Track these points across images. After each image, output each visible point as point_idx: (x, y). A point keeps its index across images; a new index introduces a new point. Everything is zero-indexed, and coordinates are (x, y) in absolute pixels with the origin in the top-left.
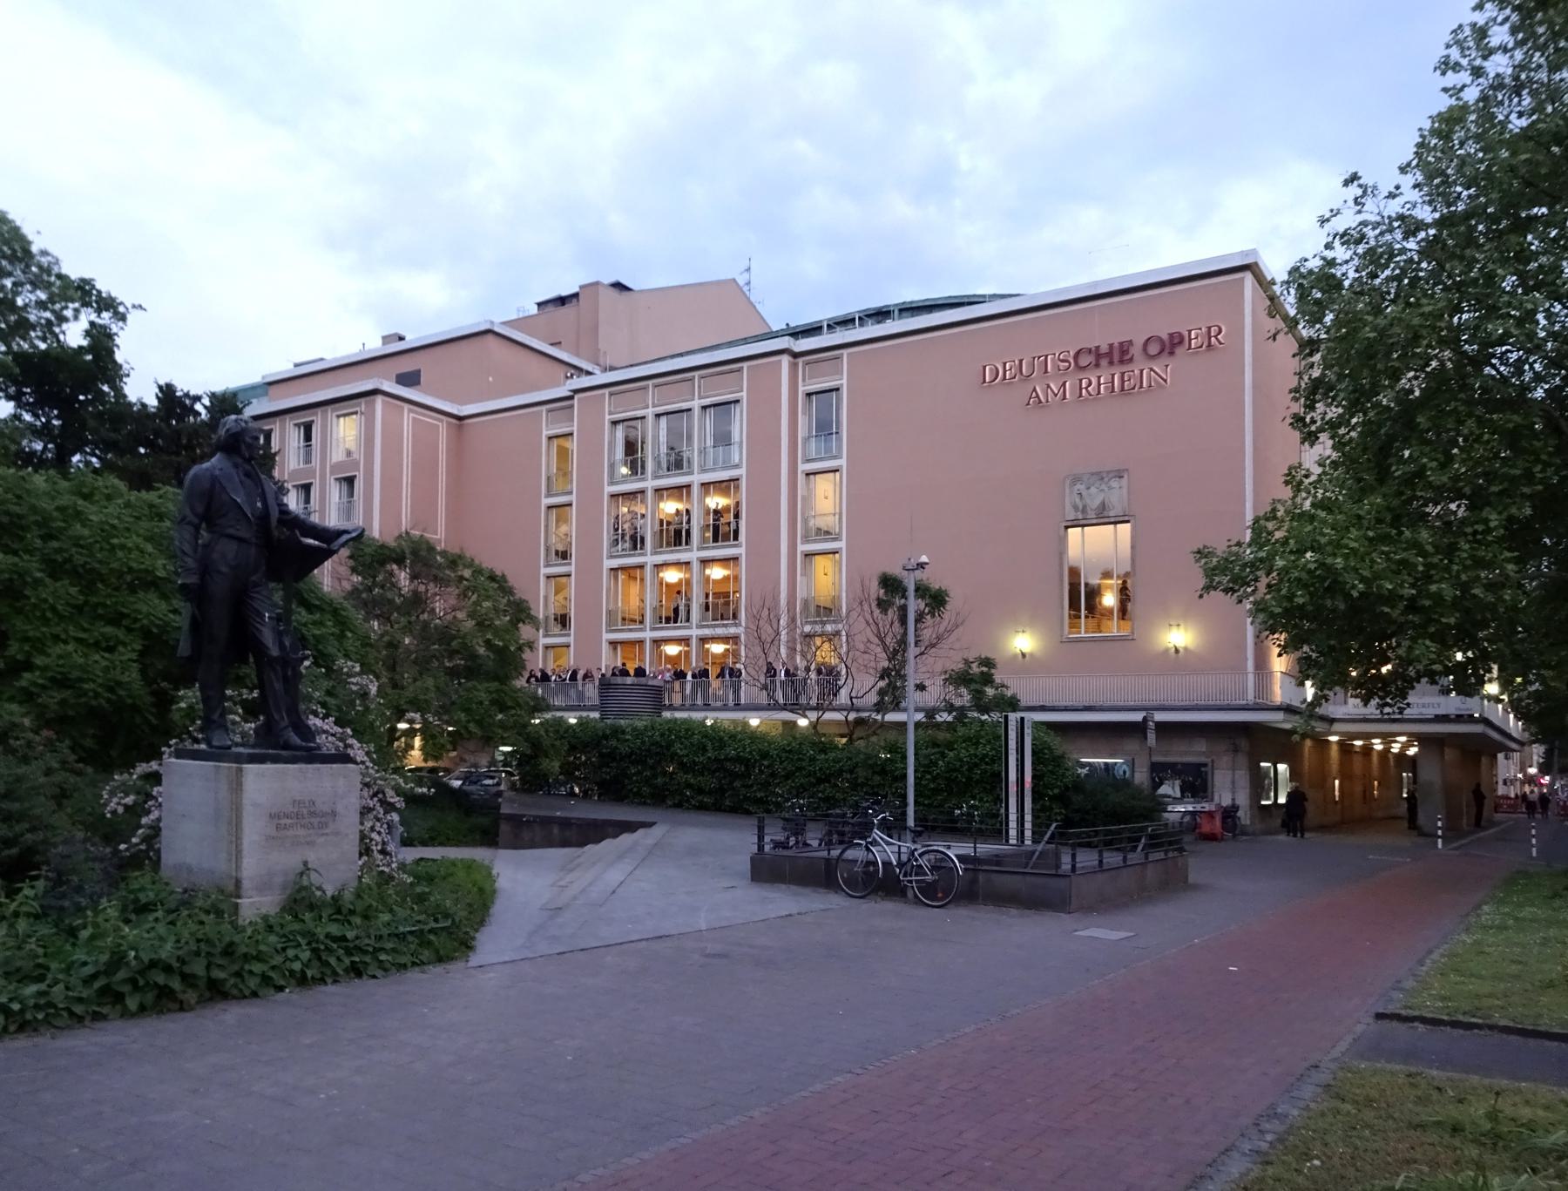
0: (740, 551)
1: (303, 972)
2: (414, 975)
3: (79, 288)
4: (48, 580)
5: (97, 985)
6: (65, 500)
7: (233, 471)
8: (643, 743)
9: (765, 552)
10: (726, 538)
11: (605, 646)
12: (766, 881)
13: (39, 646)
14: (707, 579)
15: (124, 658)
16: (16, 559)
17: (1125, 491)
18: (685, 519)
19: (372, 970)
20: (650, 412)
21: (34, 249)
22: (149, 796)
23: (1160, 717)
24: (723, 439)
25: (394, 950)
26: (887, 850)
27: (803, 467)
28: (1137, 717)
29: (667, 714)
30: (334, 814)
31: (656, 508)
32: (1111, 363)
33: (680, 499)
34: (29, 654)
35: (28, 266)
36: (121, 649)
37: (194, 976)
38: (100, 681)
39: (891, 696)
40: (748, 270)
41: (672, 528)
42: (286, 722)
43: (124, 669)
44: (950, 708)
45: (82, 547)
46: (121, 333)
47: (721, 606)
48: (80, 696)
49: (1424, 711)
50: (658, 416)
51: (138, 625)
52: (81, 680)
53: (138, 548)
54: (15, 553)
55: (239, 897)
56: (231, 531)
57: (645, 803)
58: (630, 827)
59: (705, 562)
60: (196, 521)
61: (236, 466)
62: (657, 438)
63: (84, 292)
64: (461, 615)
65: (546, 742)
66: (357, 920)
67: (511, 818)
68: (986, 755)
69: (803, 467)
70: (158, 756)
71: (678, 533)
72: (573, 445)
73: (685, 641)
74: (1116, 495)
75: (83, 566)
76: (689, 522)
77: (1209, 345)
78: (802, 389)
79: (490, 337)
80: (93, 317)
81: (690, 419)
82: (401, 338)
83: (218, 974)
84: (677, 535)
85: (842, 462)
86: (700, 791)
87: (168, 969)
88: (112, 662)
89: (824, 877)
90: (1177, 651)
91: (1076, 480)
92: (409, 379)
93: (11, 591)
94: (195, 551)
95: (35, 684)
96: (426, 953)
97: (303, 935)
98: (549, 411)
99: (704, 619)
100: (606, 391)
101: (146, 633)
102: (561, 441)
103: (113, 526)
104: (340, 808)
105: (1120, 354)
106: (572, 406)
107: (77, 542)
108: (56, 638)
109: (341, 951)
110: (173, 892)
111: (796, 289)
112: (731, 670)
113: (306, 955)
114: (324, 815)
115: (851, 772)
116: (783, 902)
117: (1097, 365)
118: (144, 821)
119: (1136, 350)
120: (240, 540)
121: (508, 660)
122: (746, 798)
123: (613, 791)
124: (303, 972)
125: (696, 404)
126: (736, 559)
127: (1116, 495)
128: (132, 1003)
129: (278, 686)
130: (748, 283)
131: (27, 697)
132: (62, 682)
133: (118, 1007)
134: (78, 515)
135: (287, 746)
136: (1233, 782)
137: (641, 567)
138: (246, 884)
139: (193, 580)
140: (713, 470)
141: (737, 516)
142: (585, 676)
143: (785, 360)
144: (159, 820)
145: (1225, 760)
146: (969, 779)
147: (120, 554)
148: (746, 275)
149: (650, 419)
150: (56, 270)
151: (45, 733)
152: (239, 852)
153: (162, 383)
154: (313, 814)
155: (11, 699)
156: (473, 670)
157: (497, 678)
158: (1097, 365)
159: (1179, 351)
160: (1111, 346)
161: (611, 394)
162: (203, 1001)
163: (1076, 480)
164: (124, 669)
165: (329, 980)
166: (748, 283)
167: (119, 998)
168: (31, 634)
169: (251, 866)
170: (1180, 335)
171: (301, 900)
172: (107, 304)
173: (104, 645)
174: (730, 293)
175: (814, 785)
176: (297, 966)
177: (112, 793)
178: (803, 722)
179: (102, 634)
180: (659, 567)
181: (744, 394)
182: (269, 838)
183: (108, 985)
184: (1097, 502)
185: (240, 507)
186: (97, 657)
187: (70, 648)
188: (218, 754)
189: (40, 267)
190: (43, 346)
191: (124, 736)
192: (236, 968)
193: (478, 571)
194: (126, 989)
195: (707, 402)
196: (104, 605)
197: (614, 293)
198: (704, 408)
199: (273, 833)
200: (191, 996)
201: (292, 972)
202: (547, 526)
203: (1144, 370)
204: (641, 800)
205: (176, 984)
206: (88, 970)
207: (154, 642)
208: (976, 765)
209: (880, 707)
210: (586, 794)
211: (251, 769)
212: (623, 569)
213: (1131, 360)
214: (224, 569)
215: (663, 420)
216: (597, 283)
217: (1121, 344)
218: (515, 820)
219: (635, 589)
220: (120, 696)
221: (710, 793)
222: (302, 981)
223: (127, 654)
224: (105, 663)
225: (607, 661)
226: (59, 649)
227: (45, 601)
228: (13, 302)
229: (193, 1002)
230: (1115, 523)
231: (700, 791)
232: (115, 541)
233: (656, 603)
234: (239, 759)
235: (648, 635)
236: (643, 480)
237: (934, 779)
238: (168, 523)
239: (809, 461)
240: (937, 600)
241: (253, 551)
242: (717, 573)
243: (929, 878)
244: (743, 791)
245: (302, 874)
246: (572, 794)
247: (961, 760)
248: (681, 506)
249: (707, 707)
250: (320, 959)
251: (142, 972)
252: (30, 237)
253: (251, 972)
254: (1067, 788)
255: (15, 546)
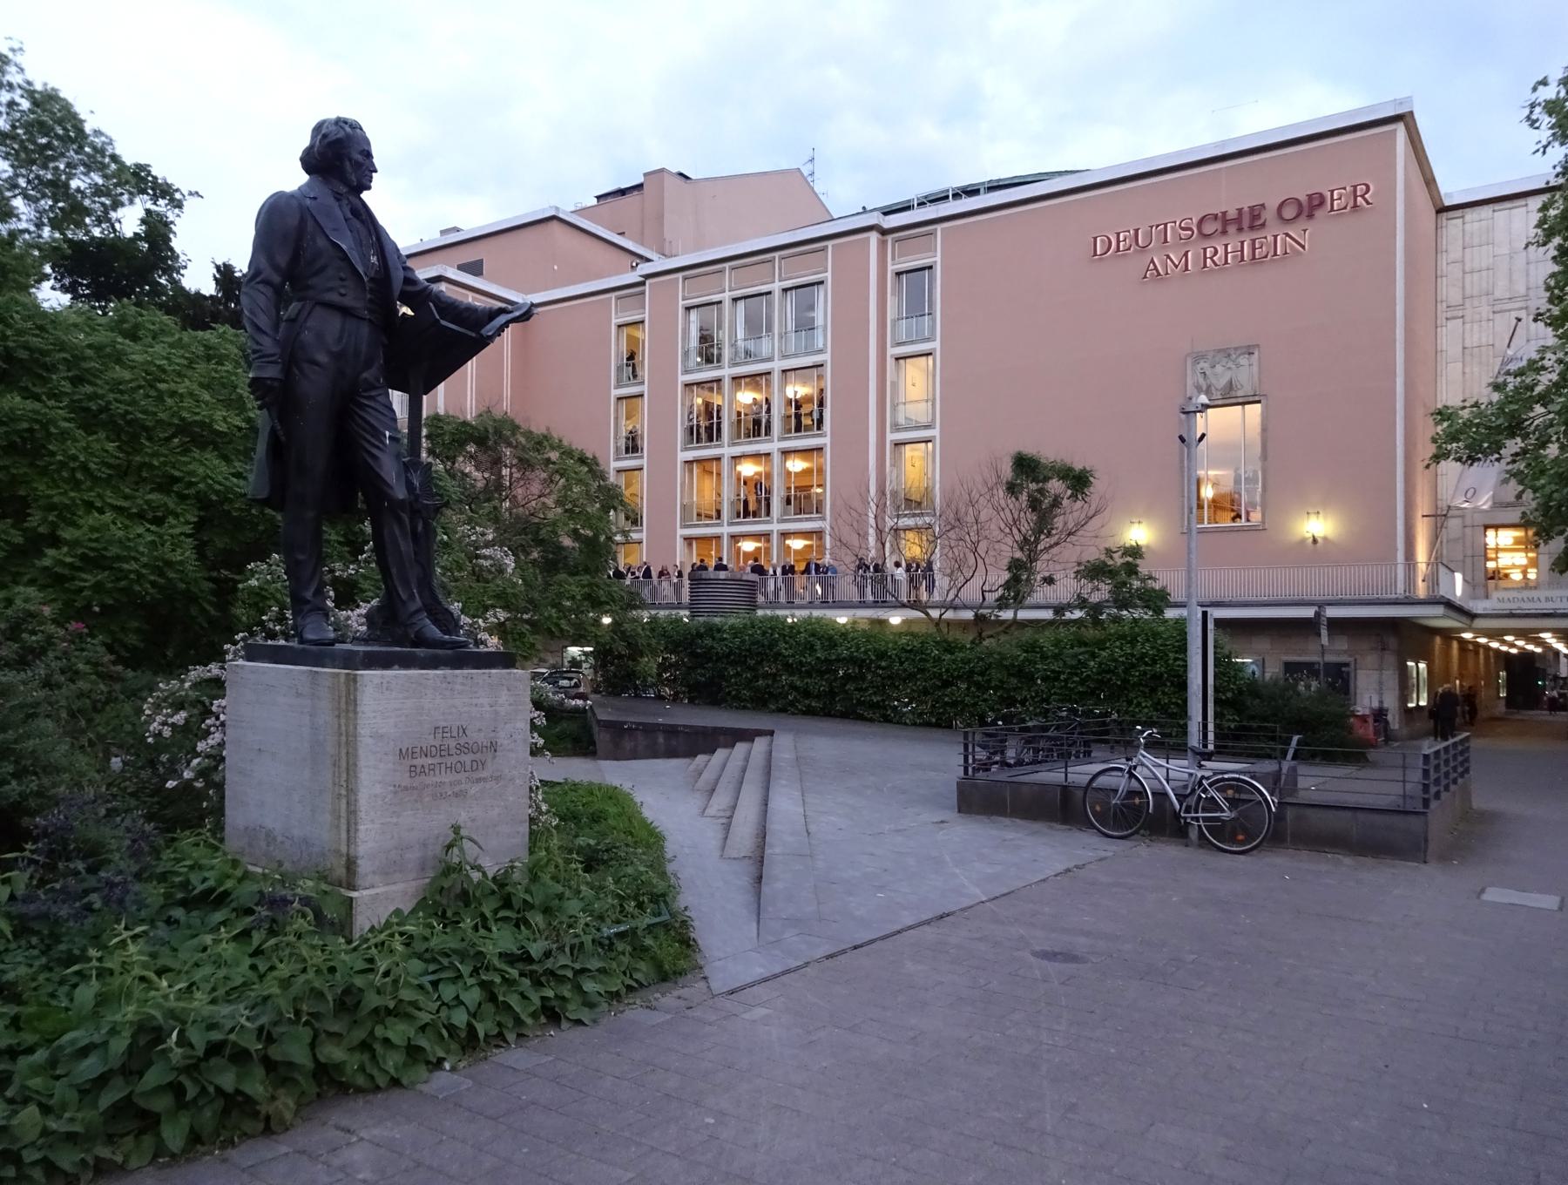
0: (825, 441)
1: (470, 1027)
2: (634, 1013)
3: (135, 174)
4: (80, 433)
5: (107, 1100)
6: (102, 337)
7: (331, 201)
8: (743, 642)
9: (852, 442)
10: (808, 428)
11: (679, 541)
12: (978, 813)
13: (66, 515)
14: (789, 473)
15: (177, 531)
16: (37, 406)
17: (1255, 369)
18: (765, 407)
19: (574, 1010)
20: (726, 297)
21: (88, 128)
22: (207, 713)
23: (1332, 612)
24: (805, 325)
25: (602, 971)
26: (1160, 773)
27: (893, 351)
28: (1309, 613)
29: (760, 613)
30: (493, 747)
31: (732, 400)
32: (1240, 230)
33: (757, 388)
34: (54, 526)
35: (81, 147)
36: (171, 520)
37: (290, 1065)
38: (144, 559)
39: (1015, 590)
40: (812, 160)
41: (751, 418)
42: (418, 603)
43: (175, 546)
44: (1082, 603)
45: (122, 392)
46: (177, 221)
47: (801, 500)
48: (118, 579)
49: (1525, 606)
50: (735, 300)
51: (192, 491)
52: (118, 558)
53: (191, 394)
54: (37, 398)
55: (353, 888)
56: (333, 297)
57: (745, 708)
58: (748, 736)
59: (786, 453)
60: (277, 279)
61: (338, 197)
62: (733, 329)
63: (140, 180)
64: (550, 502)
65: (642, 641)
66: (537, 919)
67: (608, 725)
68: (1144, 655)
69: (893, 351)
70: (219, 656)
71: (757, 422)
72: (644, 334)
73: (766, 536)
74: (1246, 374)
75: (123, 416)
76: (768, 411)
77: (1355, 206)
78: (891, 268)
79: (555, 224)
80: (149, 205)
81: (770, 305)
82: (457, 230)
83: (333, 1053)
84: (757, 427)
85: (936, 345)
86: (807, 694)
87: (240, 1057)
88: (161, 537)
89: (1065, 809)
90: (1315, 541)
91: (1198, 358)
92: (475, 268)
93: (28, 445)
94: (276, 327)
95: (61, 563)
96: (642, 966)
97: (463, 955)
98: (618, 298)
99: (785, 513)
100: (680, 275)
101: (203, 502)
102: (630, 330)
103: (161, 369)
104: (502, 739)
105: (1251, 219)
106: (643, 293)
107: (116, 386)
108: (89, 506)
109: (527, 982)
110: (246, 876)
111: (846, 195)
112: (817, 566)
113: (473, 996)
114: (481, 749)
115: (982, 674)
116: (1042, 853)
117: (1224, 232)
118: (201, 746)
119: (1269, 215)
120: (345, 312)
121: (597, 550)
122: (860, 703)
123: (708, 693)
124: (470, 1027)
125: (776, 287)
126: (820, 449)
127: (1246, 374)
128: (173, 1135)
129: (406, 546)
130: (812, 174)
131: (55, 580)
132: (94, 561)
133: (148, 1141)
134: (119, 358)
135: (420, 641)
136: (1381, 683)
137: (718, 459)
138: (364, 866)
139: (272, 372)
140: (796, 355)
141: (821, 404)
142: (661, 574)
143: (874, 237)
144: (222, 745)
145: (1371, 659)
146: (1125, 681)
147: (169, 401)
148: (810, 166)
149: (727, 304)
150: (110, 151)
151: (73, 626)
152: (352, 812)
153: (220, 263)
154: (463, 749)
155: (32, 582)
156: (554, 561)
157: (587, 571)
158: (1224, 232)
159: (1319, 213)
160: (1240, 210)
161: (685, 279)
162: (304, 1106)
163: (1198, 358)
164: (175, 546)
165: (511, 1037)
166: (812, 174)
167: (149, 1122)
168: (56, 499)
169: (370, 839)
170: (1321, 195)
171: (451, 895)
172: (163, 191)
173: (150, 515)
174: (794, 185)
175: (939, 688)
176: (460, 1018)
177: (157, 707)
178: (895, 619)
179: (147, 502)
180: (736, 459)
181: (829, 274)
182: (399, 789)
183: (129, 1097)
184: (1223, 382)
185: (345, 257)
186: (140, 530)
187: (108, 516)
188: (315, 654)
189: (94, 148)
190: (97, 232)
191: (178, 630)
192: (359, 1035)
193: (568, 453)
194: (161, 1104)
195: (788, 284)
196: (151, 466)
197: (681, 181)
198: (785, 290)
199: (407, 782)
200: (285, 1103)
201: (451, 1028)
202: (616, 418)
203: (1275, 236)
204: (761, 701)
205: (256, 1087)
206: (90, 1067)
207: (213, 513)
208: (1133, 666)
209: (1002, 603)
210: (675, 699)
211: (370, 677)
212: (698, 461)
213: (1263, 225)
214: (322, 358)
215: (741, 304)
216: (662, 170)
217: (1252, 208)
218: (616, 728)
219: (709, 484)
220: (170, 580)
221: (818, 697)
222: (470, 1043)
223: (178, 527)
224: (150, 538)
225: (683, 558)
226: (93, 519)
227: (74, 458)
228: (67, 186)
229: (288, 1116)
230: (1243, 404)
231: (807, 694)
232: (162, 386)
233: (733, 497)
234: (349, 661)
235: (725, 530)
236: (719, 368)
237: (1083, 682)
238: (229, 367)
239: (899, 344)
240: (1079, 481)
241: (365, 330)
242: (796, 465)
243: (1227, 815)
244: (857, 695)
245: (449, 847)
246: (660, 698)
247: (1115, 660)
248: (760, 397)
249: (790, 604)
250: (493, 998)
251: (193, 1068)
252: (82, 117)
253: (387, 1041)
254: (1241, 692)
255: (37, 390)
